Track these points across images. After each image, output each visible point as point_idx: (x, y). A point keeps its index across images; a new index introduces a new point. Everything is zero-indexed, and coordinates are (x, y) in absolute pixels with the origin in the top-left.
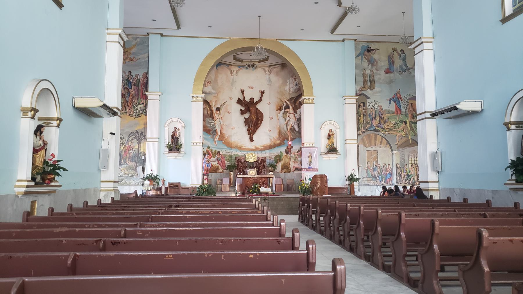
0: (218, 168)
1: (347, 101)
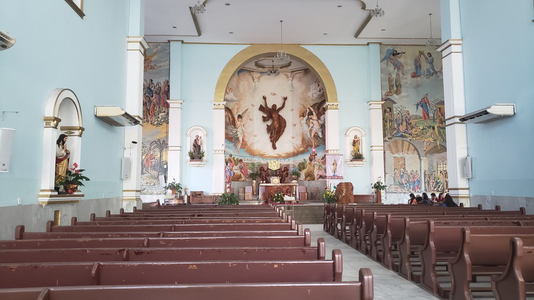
0: (240, 177)
1: (373, 106)
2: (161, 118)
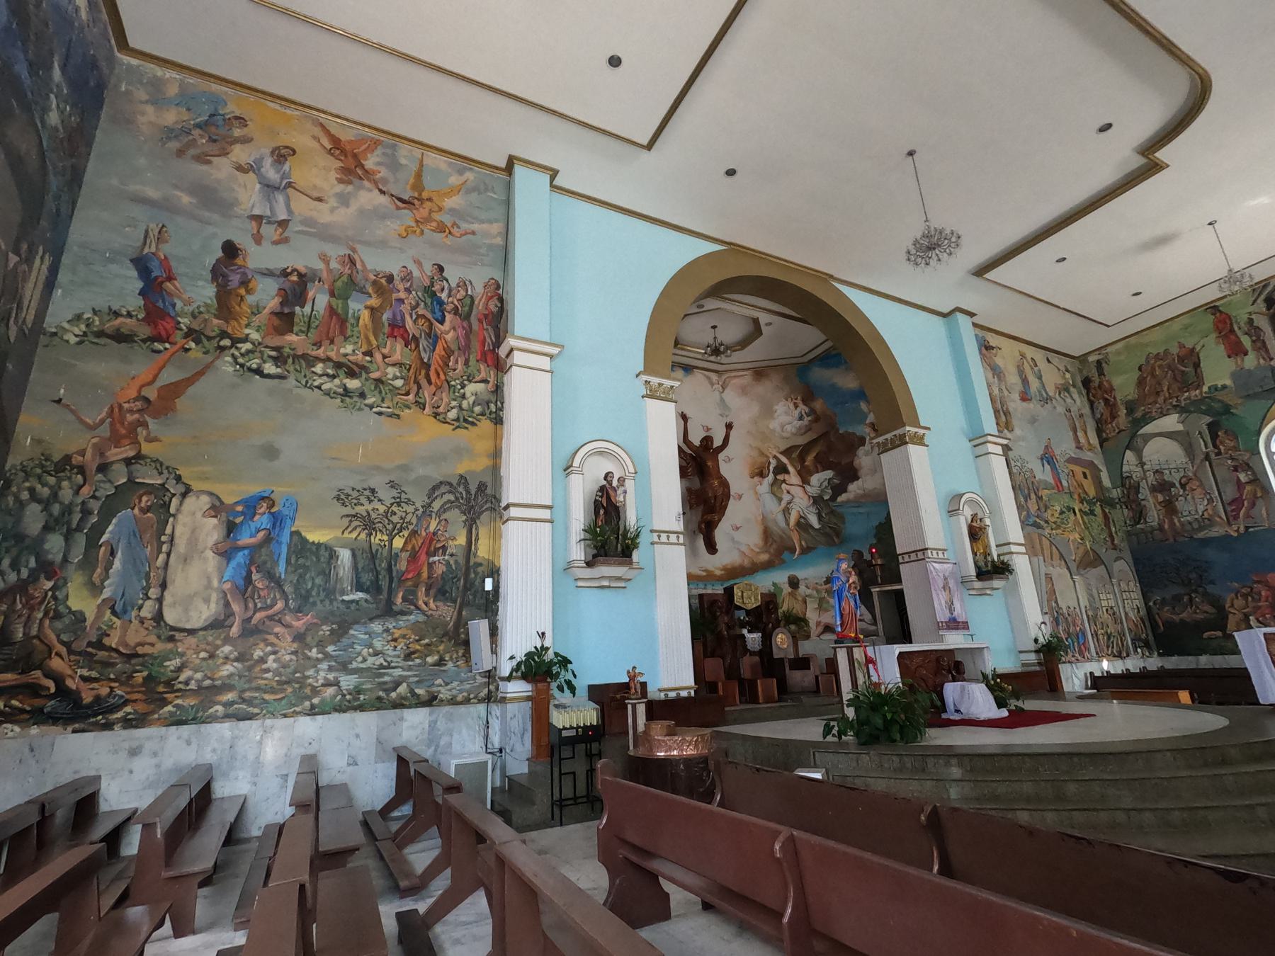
2: (474, 403)
